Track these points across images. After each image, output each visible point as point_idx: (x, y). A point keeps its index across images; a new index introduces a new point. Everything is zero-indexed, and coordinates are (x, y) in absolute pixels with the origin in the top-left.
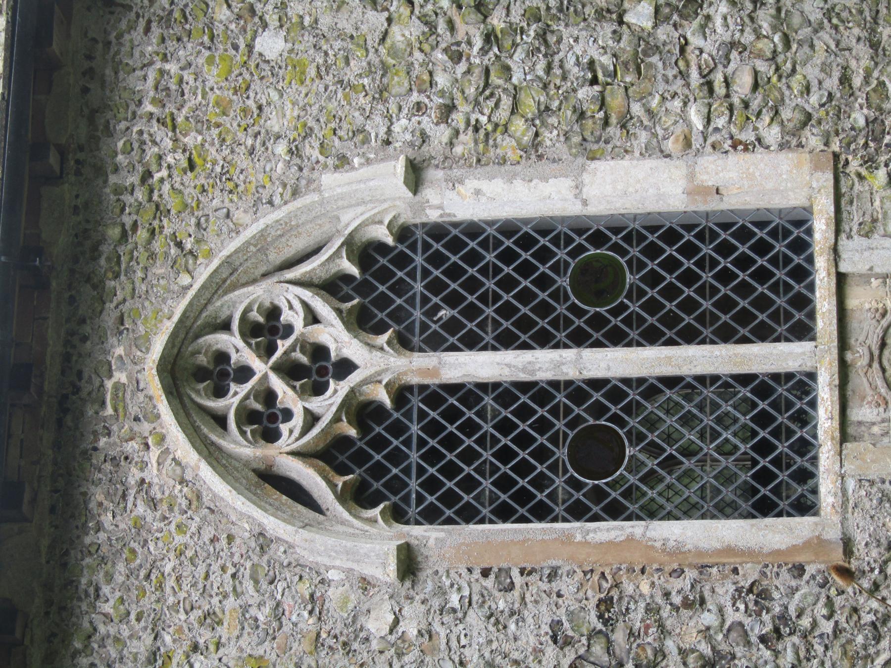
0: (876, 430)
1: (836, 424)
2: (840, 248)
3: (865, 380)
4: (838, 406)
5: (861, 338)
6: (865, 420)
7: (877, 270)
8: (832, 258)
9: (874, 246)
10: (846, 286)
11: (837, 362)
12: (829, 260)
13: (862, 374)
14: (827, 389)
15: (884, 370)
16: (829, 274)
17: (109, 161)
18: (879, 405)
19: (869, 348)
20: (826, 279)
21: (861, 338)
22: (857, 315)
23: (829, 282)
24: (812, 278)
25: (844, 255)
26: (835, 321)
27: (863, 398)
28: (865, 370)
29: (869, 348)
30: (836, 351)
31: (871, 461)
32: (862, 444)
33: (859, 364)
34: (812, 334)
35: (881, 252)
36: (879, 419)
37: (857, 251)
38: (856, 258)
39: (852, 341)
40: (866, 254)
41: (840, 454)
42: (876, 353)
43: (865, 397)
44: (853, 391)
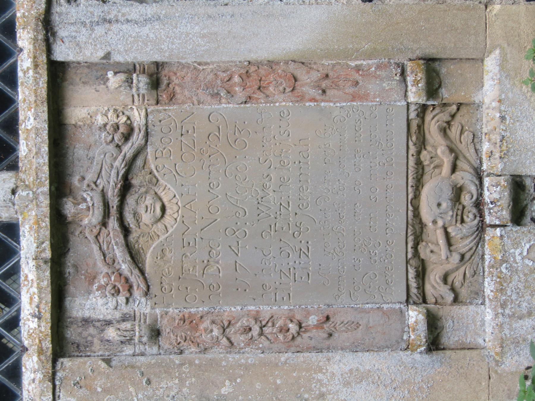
0: (111, 333)
1: (46, 327)
2: (55, 18)
3: (95, 248)
4: (50, 296)
5: (90, 177)
6: (94, 316)
7: (117, 58)
8: (41, 37)
9: (112, 16)
10: (66, 84)
11: (48, 220)
12: (35, 39)
13: (91, 238)
14: (32, 263)
15: (126, 231)
16: (36, 66)
18: (118, 292)
19: (103, 194)
20: (31, 72)
21: (90, 177)
22: (83, 135)
23: (35, 79)
24: (12, 61)
25: (62, 32)
26: (45, 149)
27: (92, 279)
28: (95, 231)
29: (103, 194)
30: (48, 202)
31: (104, 390)
32: (89, 362)
33: (86, 221)
34: (12, 157)
35: (124, 27)
36: (118, 315)
37: (84, 24)
38: (82, 38)
39: (75, 181)
40: (99, 30)
41: (53, 379)
42: (114, 202)
43: (95, 278)
44: (76, 267)
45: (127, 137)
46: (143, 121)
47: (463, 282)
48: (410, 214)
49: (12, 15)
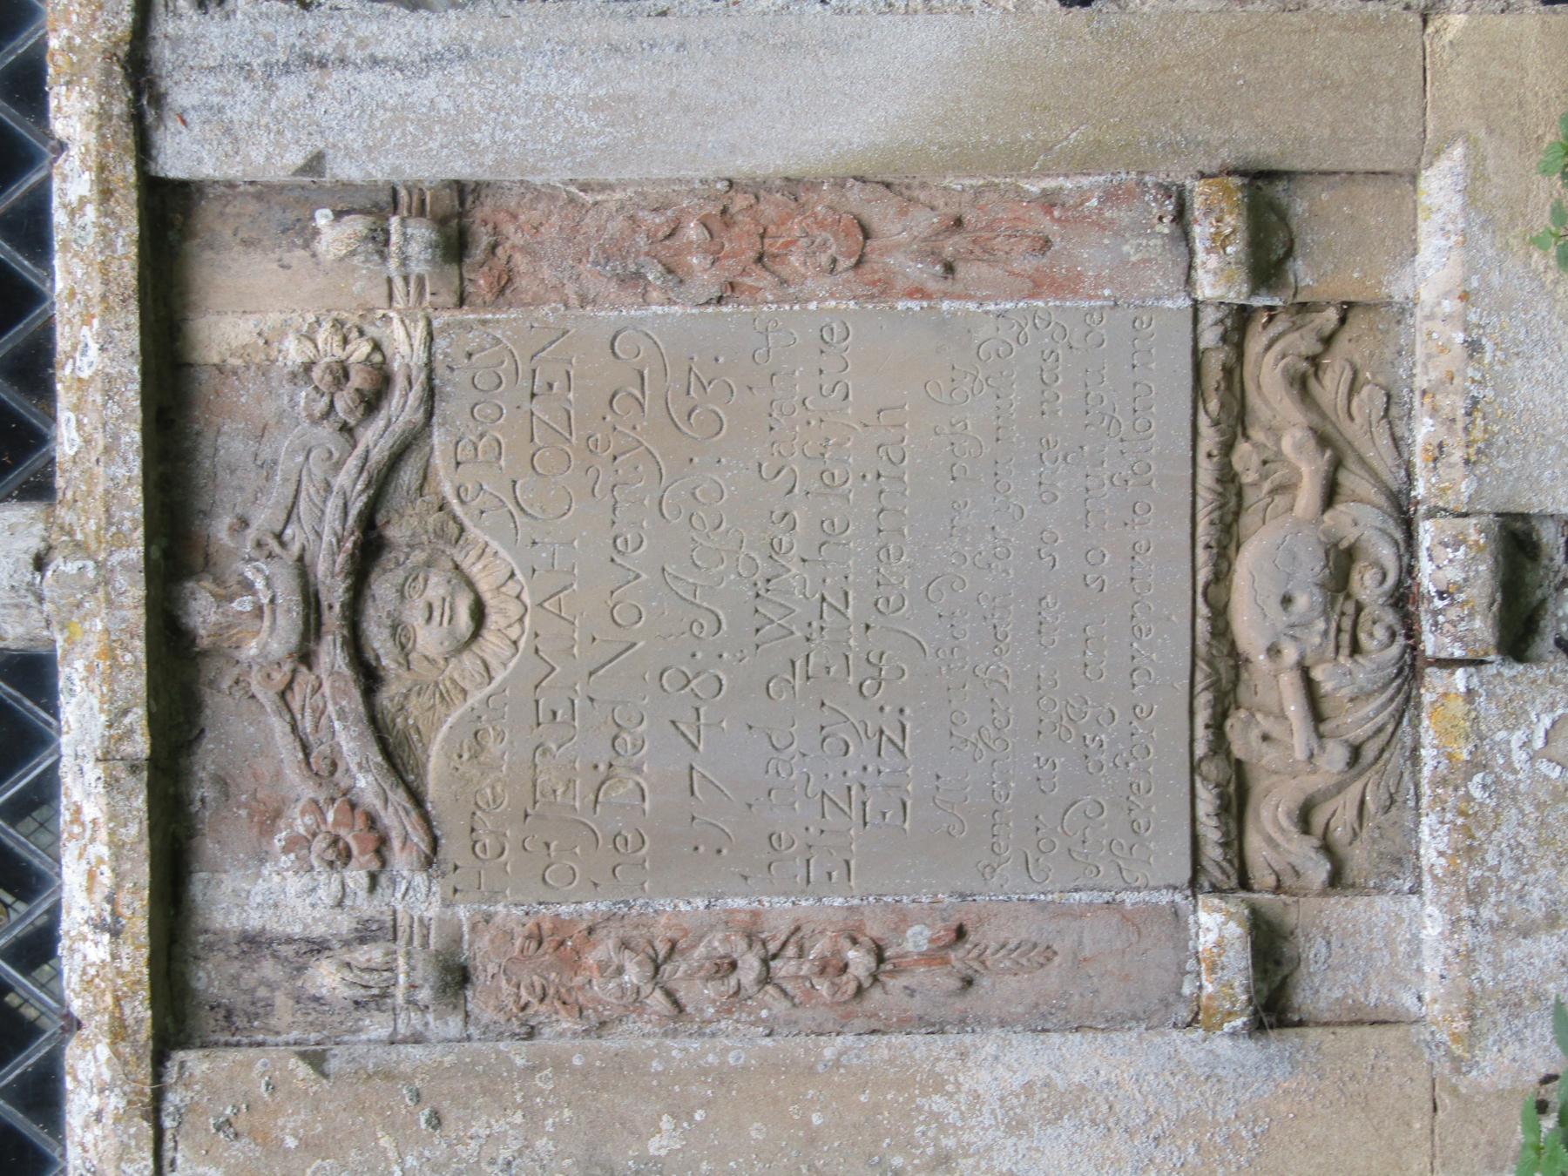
0: (326, 977)
1: (135, 959)
2: (162, 54)
3: (279, 726)
4: (145, 868)
5: (264, 518)
6: (276, 927)
7: (343, 169)
8: (119, 108)
9: (327, 47)
10: (192, 246)
11: (140, 645)
12: (103, 116)
13: (267, 697)
14: (93, 772)
15: (369, 677)
16: (106, 193)
17: (1552, 263)
18: (347, 855)
19: (303, 569)
20: (91, 212)
21: (264, 518)
22: (244, 396)
23: (104, 232)
24: (34, 178)
25: (182, 95)
26: (133, 436)
27: (270, 818)
28: (280, 678)
29: (303, 569)
30: (139, 591)
31: (306, 1145)
32: (260, 1061)
33: (251, 649)
34: (35, 462)
35: (364, 79)
36: (345, 924)
37: (245, 70)
38: (241, 111)
39: (220, 530)
40: (292, 89)
41: (155, 1112)
42: (334, 593)
43: (277, 814)
44: (222, 782)
45: (372, 402)
46: (420, 356)
47: (1356, 826)
48: (1203, 627)
49: (36, 43)
